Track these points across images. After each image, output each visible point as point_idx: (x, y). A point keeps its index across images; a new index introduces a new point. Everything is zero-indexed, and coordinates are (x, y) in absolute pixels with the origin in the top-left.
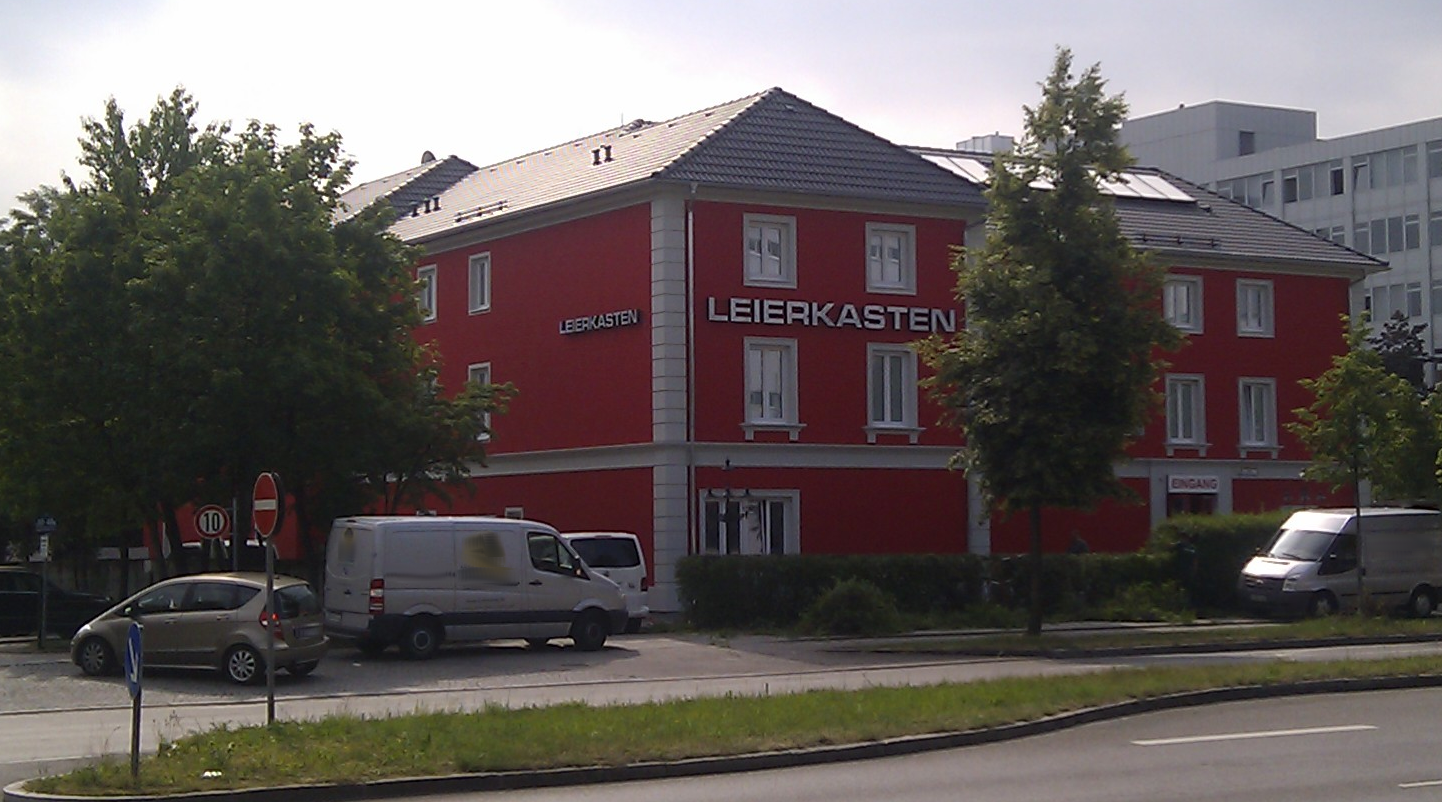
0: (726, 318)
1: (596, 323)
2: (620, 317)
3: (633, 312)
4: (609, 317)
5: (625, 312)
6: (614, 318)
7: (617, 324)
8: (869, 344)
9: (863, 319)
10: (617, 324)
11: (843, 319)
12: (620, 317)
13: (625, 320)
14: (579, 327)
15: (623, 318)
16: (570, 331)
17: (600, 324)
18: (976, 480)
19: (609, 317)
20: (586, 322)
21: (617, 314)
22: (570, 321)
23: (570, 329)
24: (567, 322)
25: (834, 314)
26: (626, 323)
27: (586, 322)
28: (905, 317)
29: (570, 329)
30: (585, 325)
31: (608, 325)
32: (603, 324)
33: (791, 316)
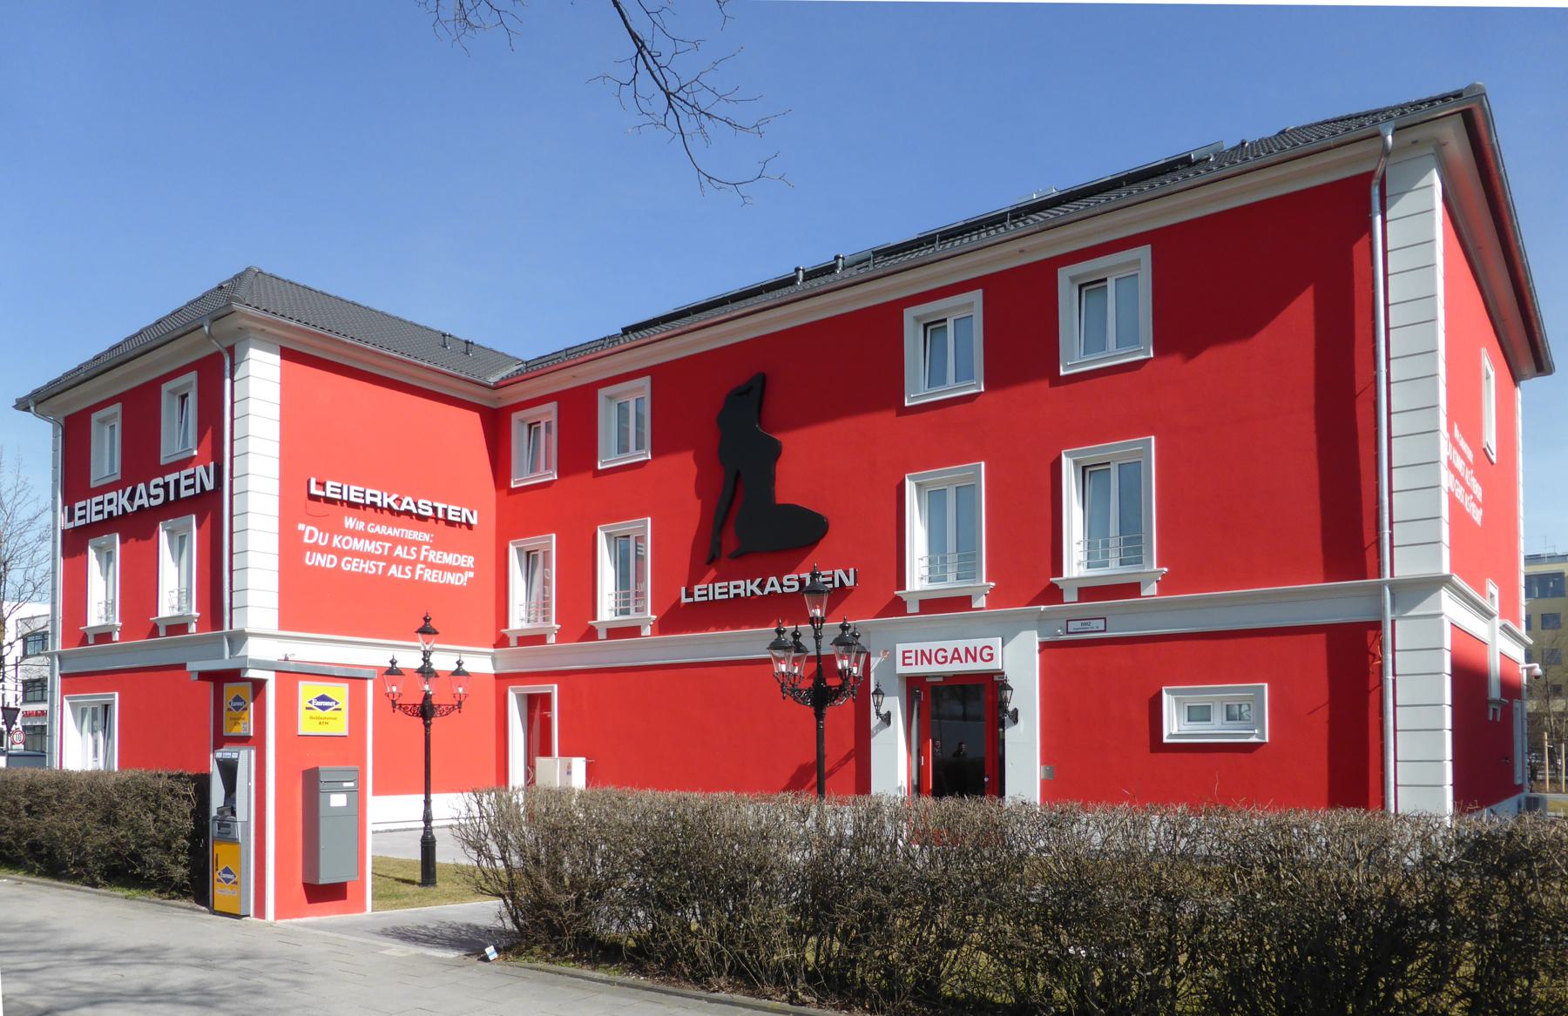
0: (370, 683)
1: (131, 498)
2: (177, 482)
3: (207, 469)
4: (156, 486)
5: (189, 471)
6: (166, 486)
7: (172, 498)
8: (301, 731)
9: (782, 586)
10: (172, 498)
11: (768, 589)
12: (177, 482)
13: (187, 488)
14: (97, 513)
15: (183, 483)
16: (83, 522)
17: (137, 502)
18: (40, 771)
19: (156, 486)
20: (110, 502)
21: (171, 478)
22: (82, 504)
23: (80, 518)
24: (77, 505)
25: (762, 586)
26: (191, 492)
27: (110, 502)
28: (445, 511)
29: (80, 518)
30: (107, 508)
31: (154, 502)
32: (145, 502)
33: (733, 592)
